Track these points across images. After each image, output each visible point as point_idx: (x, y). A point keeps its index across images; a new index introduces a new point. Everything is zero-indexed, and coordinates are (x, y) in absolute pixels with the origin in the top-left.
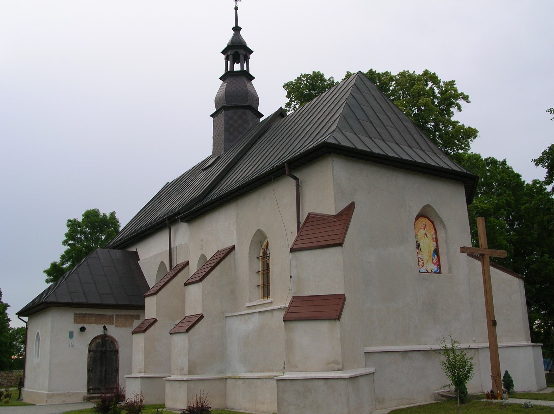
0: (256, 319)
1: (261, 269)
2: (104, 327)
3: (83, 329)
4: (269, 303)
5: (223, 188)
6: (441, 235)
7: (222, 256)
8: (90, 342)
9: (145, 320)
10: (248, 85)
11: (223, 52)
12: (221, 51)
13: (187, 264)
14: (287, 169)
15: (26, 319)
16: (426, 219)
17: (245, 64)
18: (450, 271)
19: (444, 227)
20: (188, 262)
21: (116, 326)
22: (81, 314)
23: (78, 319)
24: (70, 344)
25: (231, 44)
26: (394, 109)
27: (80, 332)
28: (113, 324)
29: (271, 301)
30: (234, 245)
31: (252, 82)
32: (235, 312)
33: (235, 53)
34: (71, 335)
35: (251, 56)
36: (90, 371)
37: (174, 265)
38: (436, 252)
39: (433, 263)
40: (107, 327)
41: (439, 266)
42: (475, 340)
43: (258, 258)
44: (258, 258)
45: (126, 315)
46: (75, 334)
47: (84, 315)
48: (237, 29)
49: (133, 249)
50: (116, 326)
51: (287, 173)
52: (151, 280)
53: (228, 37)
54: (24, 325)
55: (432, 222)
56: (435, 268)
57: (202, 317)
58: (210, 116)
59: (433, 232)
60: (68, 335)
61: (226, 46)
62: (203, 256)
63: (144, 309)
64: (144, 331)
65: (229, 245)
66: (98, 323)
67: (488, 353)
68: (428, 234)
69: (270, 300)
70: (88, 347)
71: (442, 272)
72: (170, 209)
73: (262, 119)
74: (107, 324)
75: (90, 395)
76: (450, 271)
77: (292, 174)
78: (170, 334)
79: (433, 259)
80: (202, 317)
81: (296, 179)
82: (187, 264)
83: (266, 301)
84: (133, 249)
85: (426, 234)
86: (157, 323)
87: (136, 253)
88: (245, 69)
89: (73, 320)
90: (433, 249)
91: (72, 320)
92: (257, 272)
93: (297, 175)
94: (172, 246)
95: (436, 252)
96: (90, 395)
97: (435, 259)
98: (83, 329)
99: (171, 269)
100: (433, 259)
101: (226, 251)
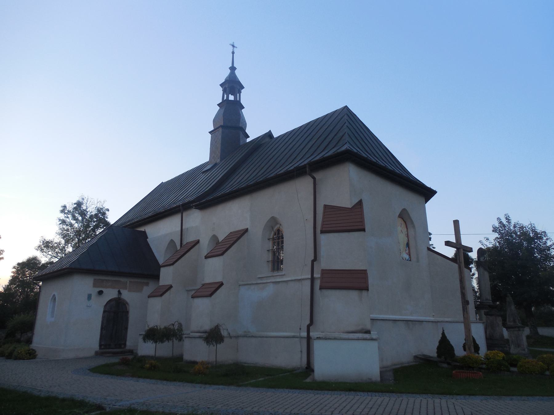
4: (282, 275)
5: (188, 196)
6: (411, 232)
7: (239, 236)
8: (105, 304)
9: (160, 286)
10: (240, 111)
12: (220, 84)
13: (198, 242)
17: (225, 98)
19: (414, 227)
20: (199, 240)
24: (88, 305)
25: (228, 79)
28: (126, 289)
29: (284, 274)
30: (248, 228)
34: (89, 297)
35: (242, 91)
36: (103, 329)
37: (184, 243)
38: (408, 245)
39: (406, 253)
41: (410, 255)
42: (434, 315)
43: (269, 239)
44: (269, 239)
46: (93, 297)
48: (233, 69)
49: (142, 229)
50: (129, 291)
51: (307, 172)
53: (225, 74)
55: (405, 222)
56: (407, 257)
57: (221, 284)
58: (209, 132)
59: (406, 230)
60: (87, 298)
62: (215, 238)
63: (159, 279)
64: (161, 295)
66: (114, 288)
69: (280, 273)
70: (103, 307)
71: (412, 260)
72: (177, 199)
73: (248, 140)
78: (192, 298)
79: (406, 250)
80: (221, 284)
81: (314, 178)
82: (198, 242)
83: (276, 273)
84: (142, 229)
85: (402, 231)
86: (172, 290)
90: (406, 243)
91: (92, 284)
92: (268, 250)
94: (184, 227)
95: (408, 245)
97: (407, 250)
99: (181, 246)
100: (406, 250)
101: (242, 233)
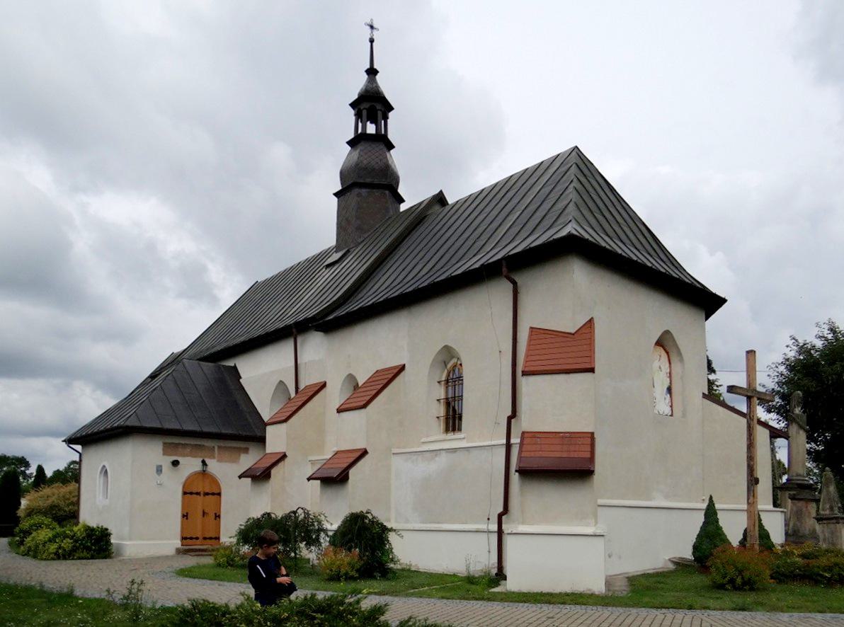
0: (443, 459)
1: (443, 396)
2: (204, 463)
3: (175, 463)
11: (353, 105)
14: (504, 269)
15: (79, 448)
16: (662, 348)
18: (684, 415)
19: (681, 360)
21: (218, 461)
22: (173, 443)
23: (168, 449)
24: (159, 482)
26: (583, 211)
27: (173, 467)
28: (214, 458)
30: (404, 365)
31: (392, 151)
32: (404, 448)
33: (371, 106)
34: (159, 470)
35: (391, 114)
37: (302, 386)
38: (669, 390)
40: (208, 461)
43: (439, 382)
44: (439, 382)
45: (231, 447)
46: (164, 469)
47: (177, 445)
48: (372, 72)
52: (265, 407)
53: (359, 82)
54: (76, 458)
55: (667, 353)
57: (364, 453)
61: (356, 97)
65: (396, 362)
67: (496, 535)
68: (662, 368)
73: (403, 207)
74: (206, 457)
75: (185, 547)
76: (684, 415)
77: (513, 277)
79: (665, 399)
81: (514, 283)
84: (230, 363)
85: (660, 368)
86: (367, 457)
87: (234, 370)
88: (383, 133)
89: (161, 451)
93: (517, 279)
96: (185, 547)
98: (175, 463)
